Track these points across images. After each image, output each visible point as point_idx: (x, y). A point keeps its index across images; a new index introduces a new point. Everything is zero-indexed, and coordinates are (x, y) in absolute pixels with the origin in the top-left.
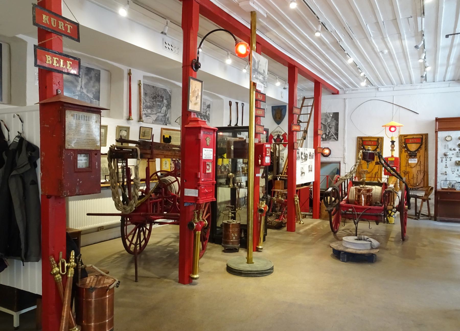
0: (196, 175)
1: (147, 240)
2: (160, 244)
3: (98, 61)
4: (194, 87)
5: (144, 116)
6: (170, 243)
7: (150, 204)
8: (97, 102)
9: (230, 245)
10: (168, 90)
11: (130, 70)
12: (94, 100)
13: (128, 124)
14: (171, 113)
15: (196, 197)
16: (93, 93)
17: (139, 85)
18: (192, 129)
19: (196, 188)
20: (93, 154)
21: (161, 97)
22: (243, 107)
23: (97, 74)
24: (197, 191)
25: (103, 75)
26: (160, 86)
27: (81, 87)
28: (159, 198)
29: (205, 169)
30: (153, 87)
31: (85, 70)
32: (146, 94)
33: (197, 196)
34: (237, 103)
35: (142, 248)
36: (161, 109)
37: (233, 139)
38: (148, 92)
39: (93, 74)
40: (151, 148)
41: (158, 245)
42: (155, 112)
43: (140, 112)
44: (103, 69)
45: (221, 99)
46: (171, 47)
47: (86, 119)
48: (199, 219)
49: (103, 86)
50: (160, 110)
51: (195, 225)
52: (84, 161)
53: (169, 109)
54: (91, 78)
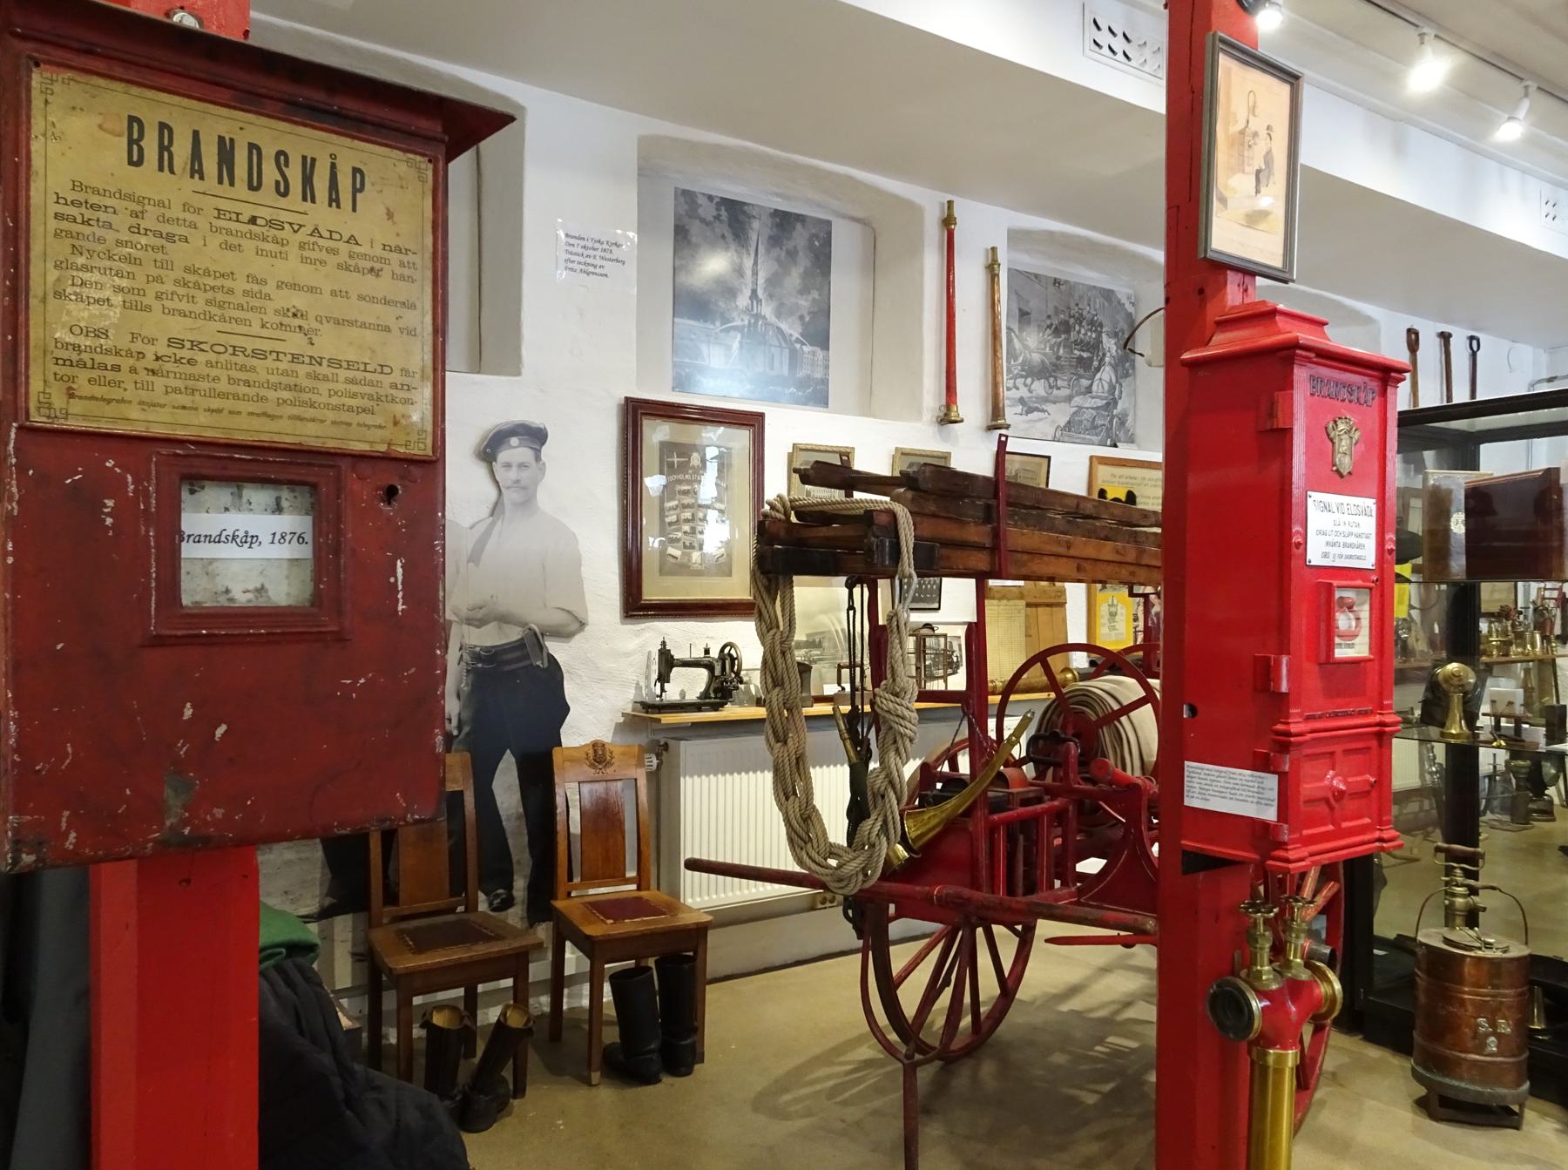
0: (1265, 672)
1: (1009, 986)
2: (1075, 1004)
3: (817, 175)
4: (1240, 111)
5: (1019, 408)
6: (1127, 1004)
7: (992, 829)
8: (820, 353)
9: (1464, 1086)
10: (1122, 291)
11: (950, 203)
12: (807, 349)
13: (945, 439)
14: (1134, 393)
15: (1264, 825)
16: (801, 318)
17: (992, 269)
18: (1238, 383)
19: (1262, 764)
20: (361, 489)
21: (1092, 323)
22: (1474, 355)
23: (816, 236)
24: (1272, 781)
25: (845, 243)
26: (1087, 275)
27: (754, 292)
28: (1052, 793)
29: (1328, 632)
30: (1057, 282)
31: (769, 221)
32: (1024, 316)
33: (1270, 814)
34: (1445, 337)
35: (985, 1028)
36: (1092, 378)
37: (1457, 481)
38: (1034, 305)
39: (800, 237)
40: (989, 515)
41: (1064, 1008)
42: (1065, 392)
43: (995, 385)
44: (844, 216)
45: (1368, 320)
46: (1119, 46)
47: (270, 173)
48: (1288, 964)
49: (845, 285)
50: (1085, 382)
51: (1257, 1005)
52: (286, 551)
53: (1127, 375)
54: (792, 254)
